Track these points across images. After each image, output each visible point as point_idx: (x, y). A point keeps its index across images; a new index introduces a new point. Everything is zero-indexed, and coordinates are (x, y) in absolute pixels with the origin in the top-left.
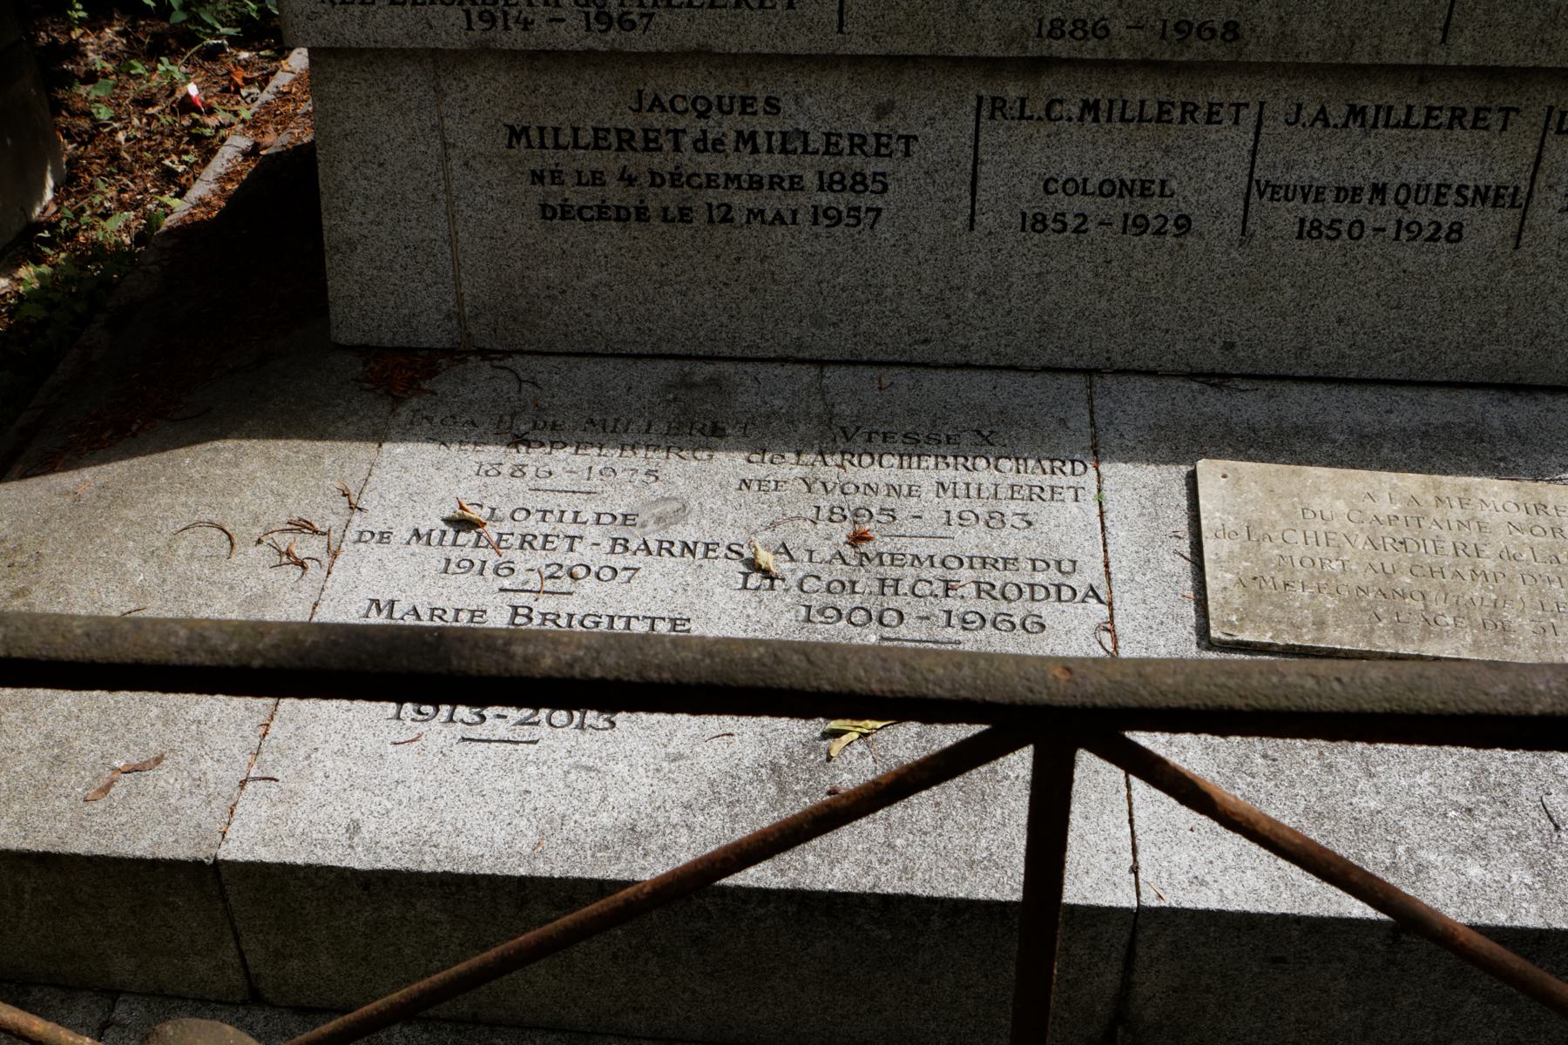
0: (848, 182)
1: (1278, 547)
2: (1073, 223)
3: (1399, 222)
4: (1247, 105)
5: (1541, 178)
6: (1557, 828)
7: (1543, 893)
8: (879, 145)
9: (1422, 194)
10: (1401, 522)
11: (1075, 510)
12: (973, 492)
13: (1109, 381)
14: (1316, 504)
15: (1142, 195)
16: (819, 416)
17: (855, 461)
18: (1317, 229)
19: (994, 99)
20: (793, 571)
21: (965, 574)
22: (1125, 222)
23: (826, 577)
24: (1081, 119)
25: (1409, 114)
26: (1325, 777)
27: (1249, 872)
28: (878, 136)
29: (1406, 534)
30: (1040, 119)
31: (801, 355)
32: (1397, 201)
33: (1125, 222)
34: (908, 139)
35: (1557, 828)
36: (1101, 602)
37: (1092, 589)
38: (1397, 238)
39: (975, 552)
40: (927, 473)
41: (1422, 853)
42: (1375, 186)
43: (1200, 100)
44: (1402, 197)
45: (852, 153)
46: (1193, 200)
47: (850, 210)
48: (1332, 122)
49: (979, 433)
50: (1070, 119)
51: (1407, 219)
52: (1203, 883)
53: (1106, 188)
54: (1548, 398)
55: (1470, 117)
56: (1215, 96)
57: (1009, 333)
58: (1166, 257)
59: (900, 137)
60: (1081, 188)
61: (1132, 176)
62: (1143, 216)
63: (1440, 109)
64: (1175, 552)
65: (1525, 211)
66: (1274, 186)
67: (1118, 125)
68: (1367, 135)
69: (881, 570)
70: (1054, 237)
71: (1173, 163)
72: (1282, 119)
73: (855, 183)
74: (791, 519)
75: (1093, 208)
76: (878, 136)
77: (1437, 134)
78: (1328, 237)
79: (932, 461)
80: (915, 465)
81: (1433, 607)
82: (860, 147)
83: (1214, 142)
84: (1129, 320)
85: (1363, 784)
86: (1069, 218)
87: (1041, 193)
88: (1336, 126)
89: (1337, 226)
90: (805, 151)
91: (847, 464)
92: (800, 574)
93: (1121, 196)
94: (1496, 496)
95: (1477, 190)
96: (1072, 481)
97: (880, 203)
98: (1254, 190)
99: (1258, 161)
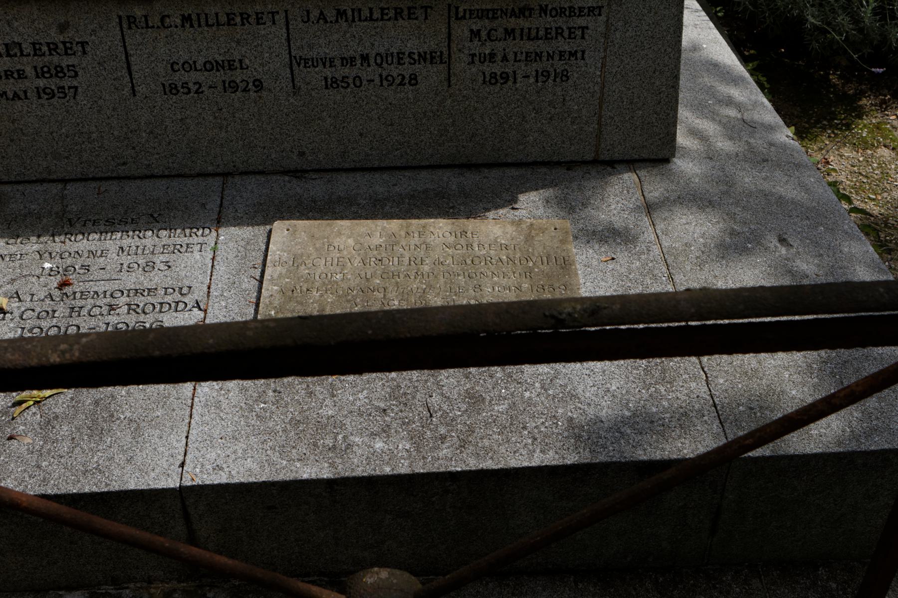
0: (53, 72)
1: (308, 269)
2: (194, 88)
3: (381, 76)
4: (278, 13)
5: (453, 45)
6: (431, 416)
7: (414, 454)
8: (66, 49)
9: (390, 59)
10: (383, 249)
11: (198, 257)
12: (140, 251)
13: (237, 180)
14: (337, 242)
15: (230, 69)
16: (57, 213)
17: (73, 239)
18: (335, 82)
19: (128, 17)
20: (19, 308)
21: (124, 299)
22: (224, 85)
23: (38, 309)
24: (183, 26)
25: (371, 13)
26: (307, 399)
27: (249, 460)
28: (64, 43)
29: (384, 255)
30: (158, 27)
31: (51, 177)
32: (377, 64)
33: (224, 85)
34: (83, 44)
35: (431, 416)
36: (200, 309)
37: (197, 303)
38: (382, 85)
39: (132, 287)
40: (113, 242)
41: (352, 438)
42: (362, 56)
43: (250, 11)
44: (379, 61)
45: (51, 54)
46: (260, 70)
47: (59, 88)
48: (329, 20)
49: (152, 215)
50: (176, 27)
51: (384, 74)
52: (221, 469)
53: (208, 66)
54: (486, 171)
55: (406, 12)
56: (258, 8)
57: (172, 155)
58: (253, 105)
59: (78, 43)
60: (193, 67)
61: (221, 58)
62: (234, 81)
63: (388, 9)
64: (251, 277)
65: (449, 65)
66: (305, 59)
67: (206, 28)
68: (350, 26)
69: (73, 302)
70: (184, 97)
71: (244, 49)
72: (299, 19)
73: (57, 72)
74: (25, 276)
75: (203, 78)
76: (64, 43)
77: (390, 24)
78: (342, 87)
79: (119, 235)
80: (109, 238)
81: (389, 295)
82: (55, 50)
83: (264, 35)
84: (241, 143)
85: (328, 402)
86: (191, 85)
87: (170, 71)
88: (331, 22)
89: (346, 80)
90: (22, 55)
91: (67, 240)
92: (23, 309)
93: (218, 70)
94: (440, 229)
95: (420, 55)
96: (201, 240)
97: (75, 83)
98: (294, 62)
99: (292, 45)
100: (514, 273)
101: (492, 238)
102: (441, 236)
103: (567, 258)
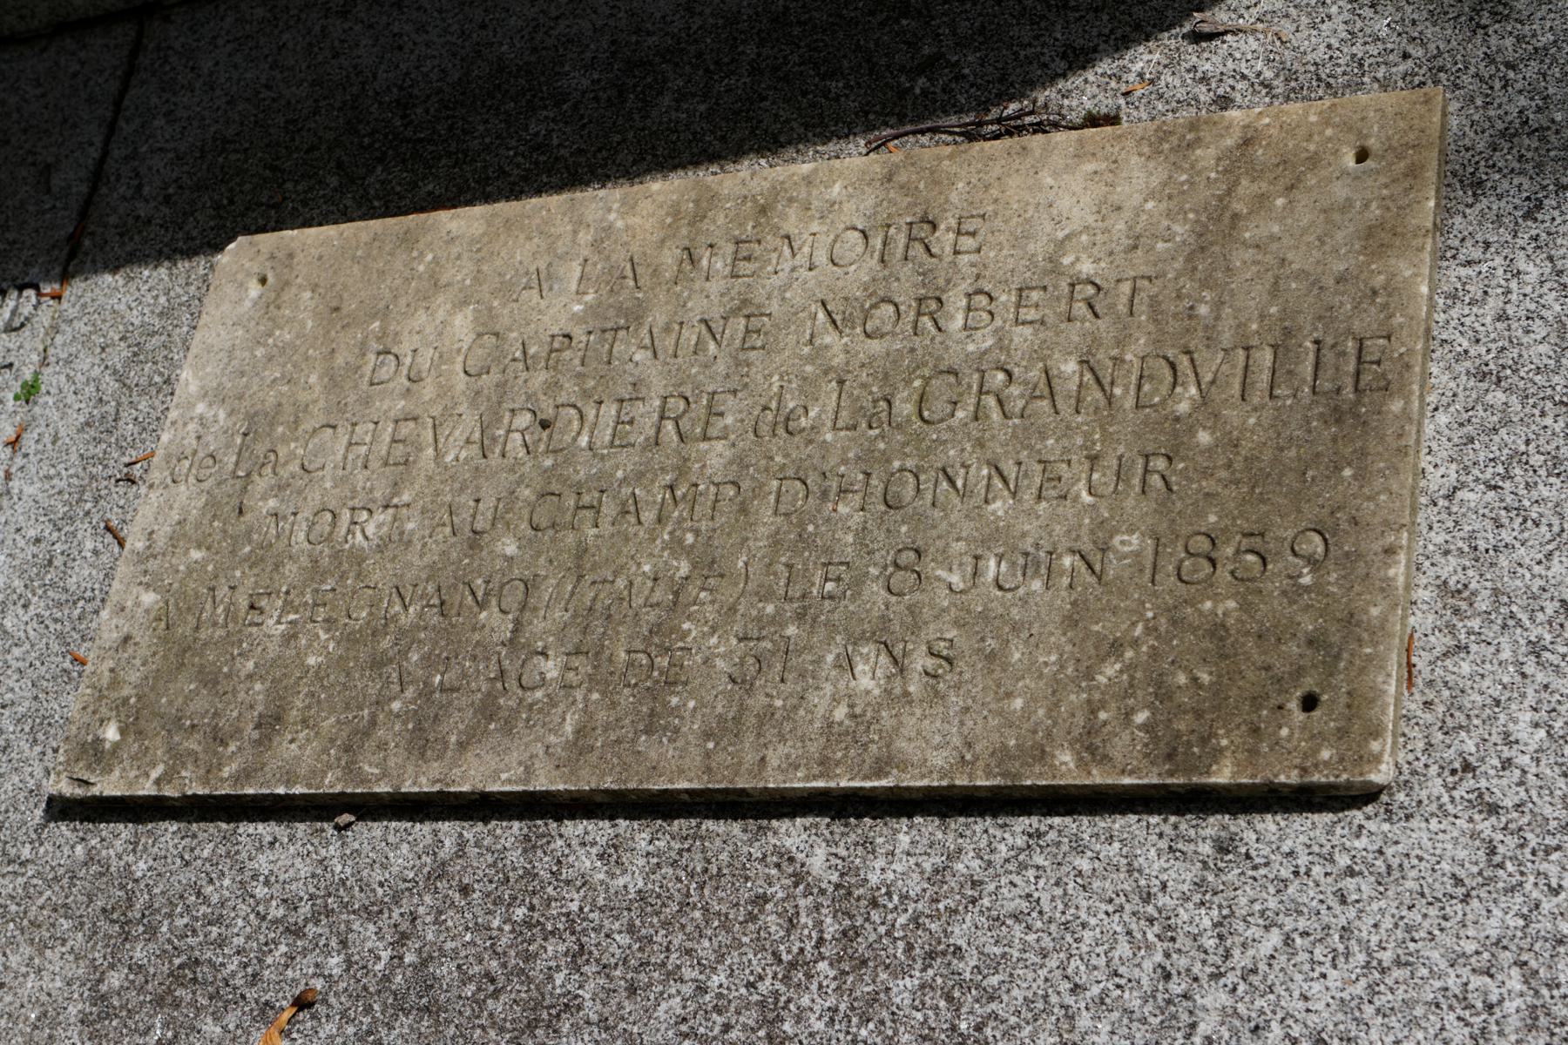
94: (827, 200)
100: (1094, 459)
101: (1038, 247)
102: (821, 258)
103: (1375, 346)
